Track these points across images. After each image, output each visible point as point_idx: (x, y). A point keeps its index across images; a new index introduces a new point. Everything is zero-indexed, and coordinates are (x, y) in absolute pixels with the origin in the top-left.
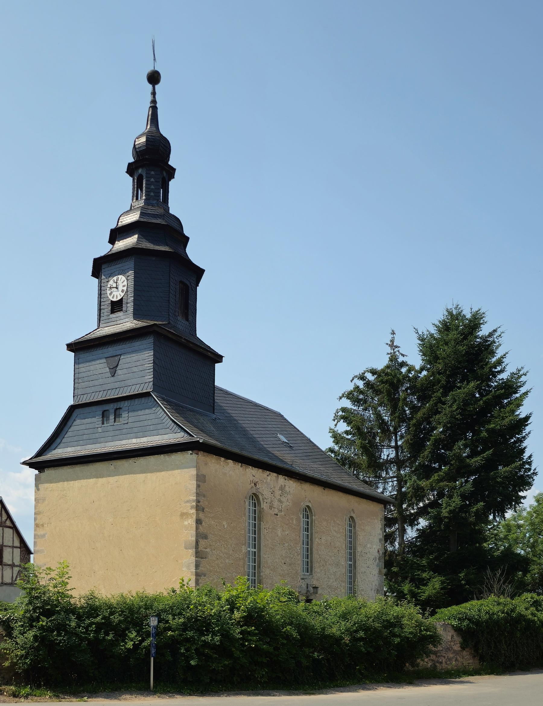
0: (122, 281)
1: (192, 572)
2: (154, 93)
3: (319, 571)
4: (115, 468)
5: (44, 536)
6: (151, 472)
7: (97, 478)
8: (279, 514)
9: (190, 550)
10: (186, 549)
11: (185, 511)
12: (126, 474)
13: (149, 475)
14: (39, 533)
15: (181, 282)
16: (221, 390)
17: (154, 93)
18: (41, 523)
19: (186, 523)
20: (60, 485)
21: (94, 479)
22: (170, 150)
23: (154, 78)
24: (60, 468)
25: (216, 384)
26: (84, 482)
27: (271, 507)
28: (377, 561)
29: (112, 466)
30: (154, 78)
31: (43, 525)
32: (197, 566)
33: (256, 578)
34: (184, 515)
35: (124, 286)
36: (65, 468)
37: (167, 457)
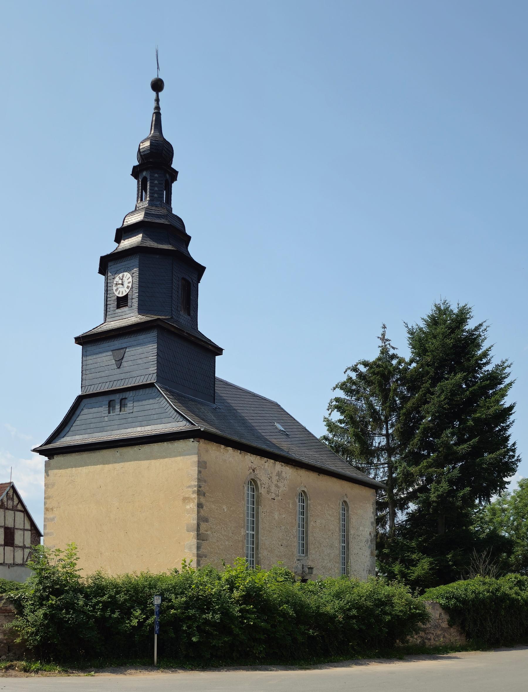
2: (157, 100)
3: (314, 552)
4: (121, 455)
8: (276, 498)
9: (192, 533)
11: (187, 496)
13: (153, 462)
15: (183, 279)
16: (221, 381)
17: (157, 100)
21: (101, 466)
23: (157, 86)
24: (69, 455)
25: (216, 375)
26: (91, 468)
27: (268, 492)
28: (369, 543)
29: (118, 453)
30: (157, 86)
32: (198, 548)
34: (186, 499)
36: (73, 455)
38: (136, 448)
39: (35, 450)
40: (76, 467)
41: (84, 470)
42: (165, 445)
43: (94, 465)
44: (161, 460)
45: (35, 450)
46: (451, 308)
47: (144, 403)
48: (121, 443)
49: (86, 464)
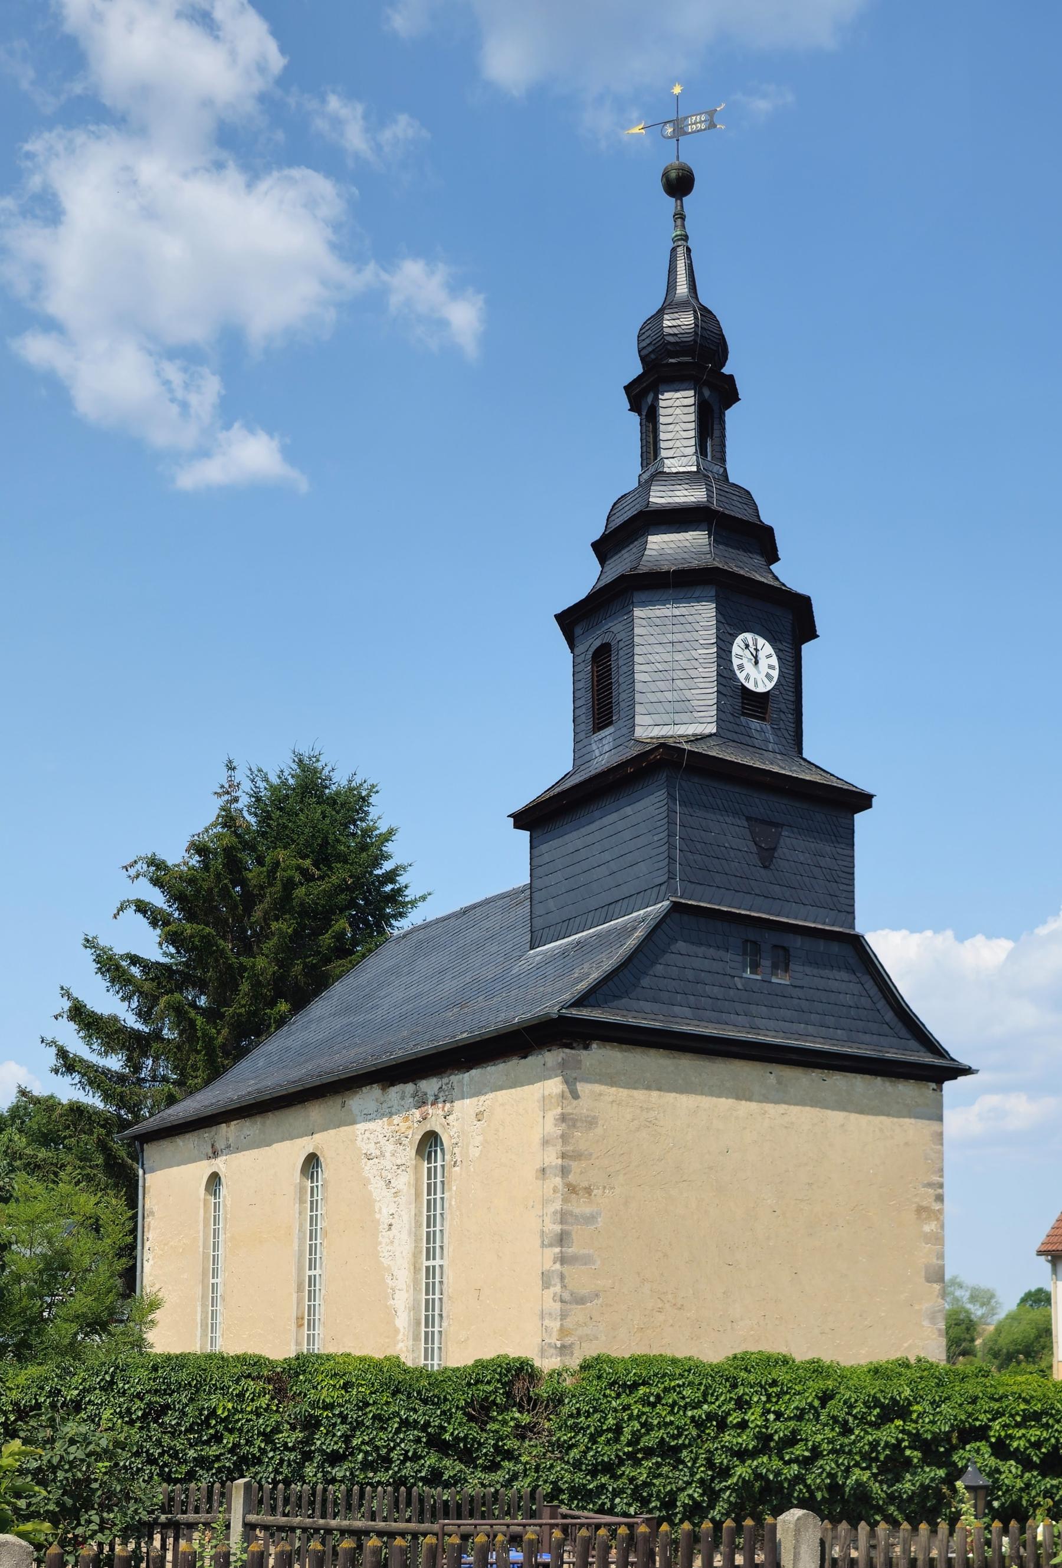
0: (760, 683)
1: (940, 1330)
2: (680, 216)
4: (779, 1083)
5: (591, 1219)
6: (861, 1112)
7: (738, 1098)
9: (935, 1285)
10: (928, 1281)
11: (924, 1204)
12: (802, 1103)
13: (853, 1117)
14: (577, 1211)
17: (680, 216)
18: (585, 1184)
19: (927, 1228)
20: (639, 1095)
21: (731, 1101)
22: (726, 359)
23: (679, 184)
24: (639, 1050)
26: (706, 1102)
29: (772, 1076)
30: (679, 184)
31: (588, 1191)
33: (309, 1214)
35: (747, 678)
36: (653, 1052)
37: (888, 1084)
38: (816, 1075)
39: (967, 1071)
40: (659, 1089)
41: (686, 1102)
42: (878, 1083)
43: (711, 1094)
44: (871, 1118)
45: (967, 1071)
46: (371, 809)
47: (826, 973)
48: (794, 1057)
49: (686, 1088)
